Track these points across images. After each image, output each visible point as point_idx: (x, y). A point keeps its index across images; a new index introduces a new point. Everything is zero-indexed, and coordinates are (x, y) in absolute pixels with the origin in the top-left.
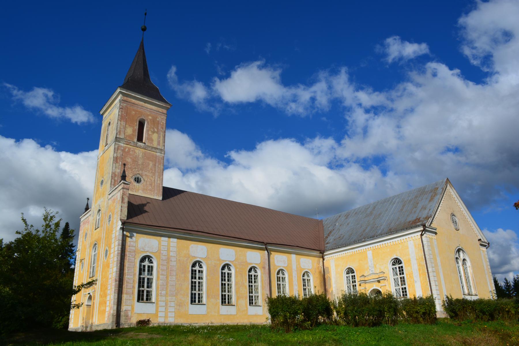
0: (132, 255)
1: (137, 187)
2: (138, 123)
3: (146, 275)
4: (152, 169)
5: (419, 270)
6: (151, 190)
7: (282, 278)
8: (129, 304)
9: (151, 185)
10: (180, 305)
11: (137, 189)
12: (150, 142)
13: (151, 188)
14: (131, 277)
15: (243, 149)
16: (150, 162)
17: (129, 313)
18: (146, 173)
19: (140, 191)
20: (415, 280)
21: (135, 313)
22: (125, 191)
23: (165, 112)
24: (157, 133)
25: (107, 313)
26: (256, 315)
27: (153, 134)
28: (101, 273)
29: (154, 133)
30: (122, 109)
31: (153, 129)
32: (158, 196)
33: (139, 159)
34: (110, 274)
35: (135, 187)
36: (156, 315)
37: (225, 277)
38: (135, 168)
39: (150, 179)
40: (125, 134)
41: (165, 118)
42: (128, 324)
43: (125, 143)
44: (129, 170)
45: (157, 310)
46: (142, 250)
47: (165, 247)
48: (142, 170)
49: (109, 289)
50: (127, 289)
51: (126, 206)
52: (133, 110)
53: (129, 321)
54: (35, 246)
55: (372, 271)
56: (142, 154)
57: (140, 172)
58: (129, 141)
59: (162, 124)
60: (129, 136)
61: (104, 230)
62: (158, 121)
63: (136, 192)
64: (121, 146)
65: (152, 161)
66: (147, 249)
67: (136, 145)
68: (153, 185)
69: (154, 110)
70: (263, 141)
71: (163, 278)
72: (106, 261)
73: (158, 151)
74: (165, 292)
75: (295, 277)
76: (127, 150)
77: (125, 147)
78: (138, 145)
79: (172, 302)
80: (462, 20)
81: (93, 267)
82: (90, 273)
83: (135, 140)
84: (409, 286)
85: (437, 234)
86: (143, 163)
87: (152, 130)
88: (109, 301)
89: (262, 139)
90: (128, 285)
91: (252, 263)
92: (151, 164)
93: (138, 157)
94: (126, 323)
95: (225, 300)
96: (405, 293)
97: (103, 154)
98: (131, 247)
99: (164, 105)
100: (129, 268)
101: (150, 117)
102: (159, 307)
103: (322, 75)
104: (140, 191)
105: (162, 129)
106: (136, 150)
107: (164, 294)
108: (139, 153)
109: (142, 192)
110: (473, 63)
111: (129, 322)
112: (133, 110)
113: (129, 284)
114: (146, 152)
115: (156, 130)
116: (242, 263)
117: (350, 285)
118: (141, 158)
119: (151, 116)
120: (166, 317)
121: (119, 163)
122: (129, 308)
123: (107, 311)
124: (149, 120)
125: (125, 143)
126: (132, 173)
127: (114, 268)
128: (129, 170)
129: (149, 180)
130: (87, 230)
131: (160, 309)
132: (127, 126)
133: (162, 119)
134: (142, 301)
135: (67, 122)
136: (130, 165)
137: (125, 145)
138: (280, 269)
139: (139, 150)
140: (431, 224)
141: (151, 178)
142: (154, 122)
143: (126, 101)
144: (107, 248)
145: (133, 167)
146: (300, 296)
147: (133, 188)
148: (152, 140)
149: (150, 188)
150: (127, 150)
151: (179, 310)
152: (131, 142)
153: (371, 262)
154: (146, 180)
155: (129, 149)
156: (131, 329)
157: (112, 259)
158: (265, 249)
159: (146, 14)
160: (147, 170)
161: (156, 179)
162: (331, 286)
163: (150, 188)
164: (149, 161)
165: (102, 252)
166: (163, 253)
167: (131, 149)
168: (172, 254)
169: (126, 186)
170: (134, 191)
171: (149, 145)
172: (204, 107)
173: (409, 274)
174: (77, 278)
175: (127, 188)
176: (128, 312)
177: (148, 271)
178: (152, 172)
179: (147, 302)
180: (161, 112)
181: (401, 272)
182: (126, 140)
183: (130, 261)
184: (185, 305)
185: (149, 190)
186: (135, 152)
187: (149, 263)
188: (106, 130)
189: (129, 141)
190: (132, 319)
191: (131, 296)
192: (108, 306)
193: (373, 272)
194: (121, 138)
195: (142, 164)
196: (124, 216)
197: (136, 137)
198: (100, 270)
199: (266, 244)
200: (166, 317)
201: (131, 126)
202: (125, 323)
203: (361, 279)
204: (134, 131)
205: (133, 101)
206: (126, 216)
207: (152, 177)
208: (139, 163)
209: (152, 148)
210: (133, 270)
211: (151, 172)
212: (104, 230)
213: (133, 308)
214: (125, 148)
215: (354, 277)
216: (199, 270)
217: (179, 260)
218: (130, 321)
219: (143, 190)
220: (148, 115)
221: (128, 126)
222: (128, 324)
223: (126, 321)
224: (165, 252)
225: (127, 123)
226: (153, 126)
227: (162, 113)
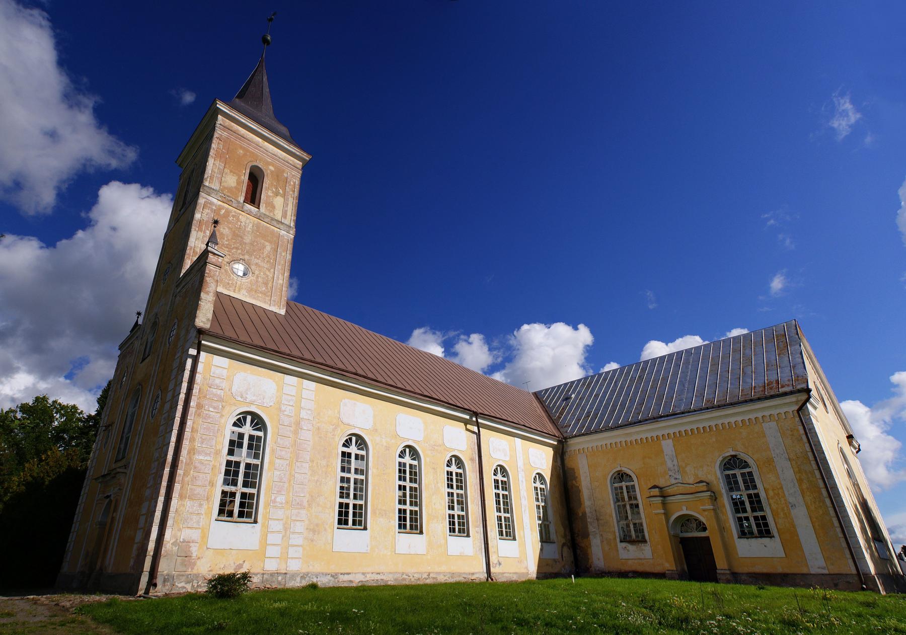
0: (214, 408)
1: (239, 283)
2: (248, 171)
3: (742, 495)
4: (269, 257)
5: (800, 481)
6: (264, 294)
7: (500, 512)
8: (195, 525)
9: (266, 284)
10: (315, 529)
11: (237, 286)
12: (268, 208)
13: (265, 290)
14: (208, 458)
15: (170, 196)
16: (267, 244)
17: (194, 550)
18: (256, 261)
19: (244, 292)
20: (790, 503)
21: (602, 535)
22: (212, 270)
23: (298, 166)
24: (284, 196)
25: (135, 546)
26: (462, 557)
27: (276, 198)
28: (138, 449)
29: (277, 196)
30: (220, 140)
31: (276, 188)
32: (277, 307)
33: (246, 234)
34: (157, 449)
35: (234, 282)
36: (261, 554)
37: (456, 481)
38: (237, 248)
39: (265, 274)
40: (222, 185)
41: (299, 176)
42: (188, 577)
43: (220, 199)
44: (223, 248)
45: (264, 543)
46: (239, 399)
47: (290, 398)
48: (251, 255)
49: (149, 486)
50: (194, 487)
51: (210, 300)
52: (241, 147)
53: (190, 570)
54: (813, 505)
55: (676, 479)
56: (253, 226)
57: (246, 257)
58: (229, 198)
59: (292, 183)
60: (230, 189)
61: (158, 358)
62: (287, 178)
63: (235, 292)
64: (212, 203)
65: (270, 242)
66: (250, 398)
67: (243, 208)
68: (270, 285)
69: (279, 158)
70: (298, 288)
71: (282, 466)
72: (153, 421)
73: (282, 227)
74: (283, 497)
75: (522, 481)
76: (223, 212)
77: (219, 205)
78: (245, 208)
79: (298, 523)
80: (295, 277)
81: (126, 438)
82: (119, 452)
83: (242, 199)
84: (775, 514)
85: (340, 498)
86: (254, 242)
87: (274, 190)
88: (144, 517)
89: (732, 329)
90: (199, 477)
91: (409, 440)
92: (268, 247)
93: (245, 229)
94: (183, 575)
95: (458, 527)
96: (343, 518)
97: (175, 224)
98: (214, 390)
99: (298, 153)
100: (204, 437)
101: (272, 168)
102: (279, 542)
103: (151, 189)
104: (244, 292)
105: (291, 193)
106: (240, 217)
107: (282, 503)
108: (246, 223)
109: (247, 294)
110: (207, 293)
111: (189, 571)
112: (241, 147)
113: (201, 475)
114: (260, 223)
115: (281, 191)
116: (436, 447)
117: (623, 503)
118: (250, 233)
119: (273, 166)
120: (285, 557)
121: (205, 232)
122: (194, 535)
123: (137, 543)
124: (269, 171)
125: (220, 199)
126: (229, 255)
127: (476, 428)
128: (225, 249)
129: (262, 274)
130: (127, 367)
131: (271, 538)
132: (226, 170)
133: (294, 175)
134: (229, 519)
135: (667, 340)
136: (226, 241)
137: (220, 203)
138: (696, 520)
139: (247, 218)
140: (726, 570)
141: (268, 273)
142: (278, 176)
143: (229, 129)
144: (160, 393)
145: (233, 246)
146: (627, 551)
147: (229, 284)
148: (274, 207)
149: (264, 289)
150: (223, 212)
151: (312, 541)
152: (233, 200)
153: (673, 461)
154: (257, 272)
155: (228, 212)
156: (99, 413)
157: (166, 415)
158: (476, 424)
159: (765, 546)
160: (260, 256)
161: (275, 276)
162: (581, 504)
163: (264, 289)
164: (265, 241)
165: (147, 402)
166: (285, 411)
167: (231, 212)
168: (303, 414)
169: (214, 260)
170: (231, 289)
171: (267, 213)
172: (17, 363)
173: (773, 490)
174: (87, 491)
175: (218, 264)
176: (191, 544)
177: (250, 447)
178: (270, 262)
179: (354, 527)
180: (293, 164)
181: (344, 510)
182: (223, 195)
183: (209, 421)
184: (325, 530)
185: (261, 292)
186: (238, 219)
187: (253, 430)
188: (792, 361)
189: (229, 198)
190: (199, 563)
191: (202, 505)
192: (141, 528)
193: (677, 481)
194: (213, 189)
195: (252, 244)
196: (204, 320)
197: (244, 194)
198: (118, 522)
199: (476, 414)
200: (285, 557)
201: (234, 173)
202: (178, 575)
203: (652, 494)
204: (239, 182)
205: (243, 131)
206: (208, 320)
207: (269, 271)
208: (245, 241)
209: (272, 219)
210: (214, 441)
211: (267, 262)
212: (158, 358)
213: (205, 536)
214: (220, 208)
215: (631, 489)
216: (355, 479)
217: (319, 429)
218: (192, 569)
219: (250, 291)
220: (268, 164)
221: (229, 171)
222: (188, 577)
223: (184, 569)
224: (291, 408)
225: (227, 166)
226: (275, 184)
227: (294, 167)
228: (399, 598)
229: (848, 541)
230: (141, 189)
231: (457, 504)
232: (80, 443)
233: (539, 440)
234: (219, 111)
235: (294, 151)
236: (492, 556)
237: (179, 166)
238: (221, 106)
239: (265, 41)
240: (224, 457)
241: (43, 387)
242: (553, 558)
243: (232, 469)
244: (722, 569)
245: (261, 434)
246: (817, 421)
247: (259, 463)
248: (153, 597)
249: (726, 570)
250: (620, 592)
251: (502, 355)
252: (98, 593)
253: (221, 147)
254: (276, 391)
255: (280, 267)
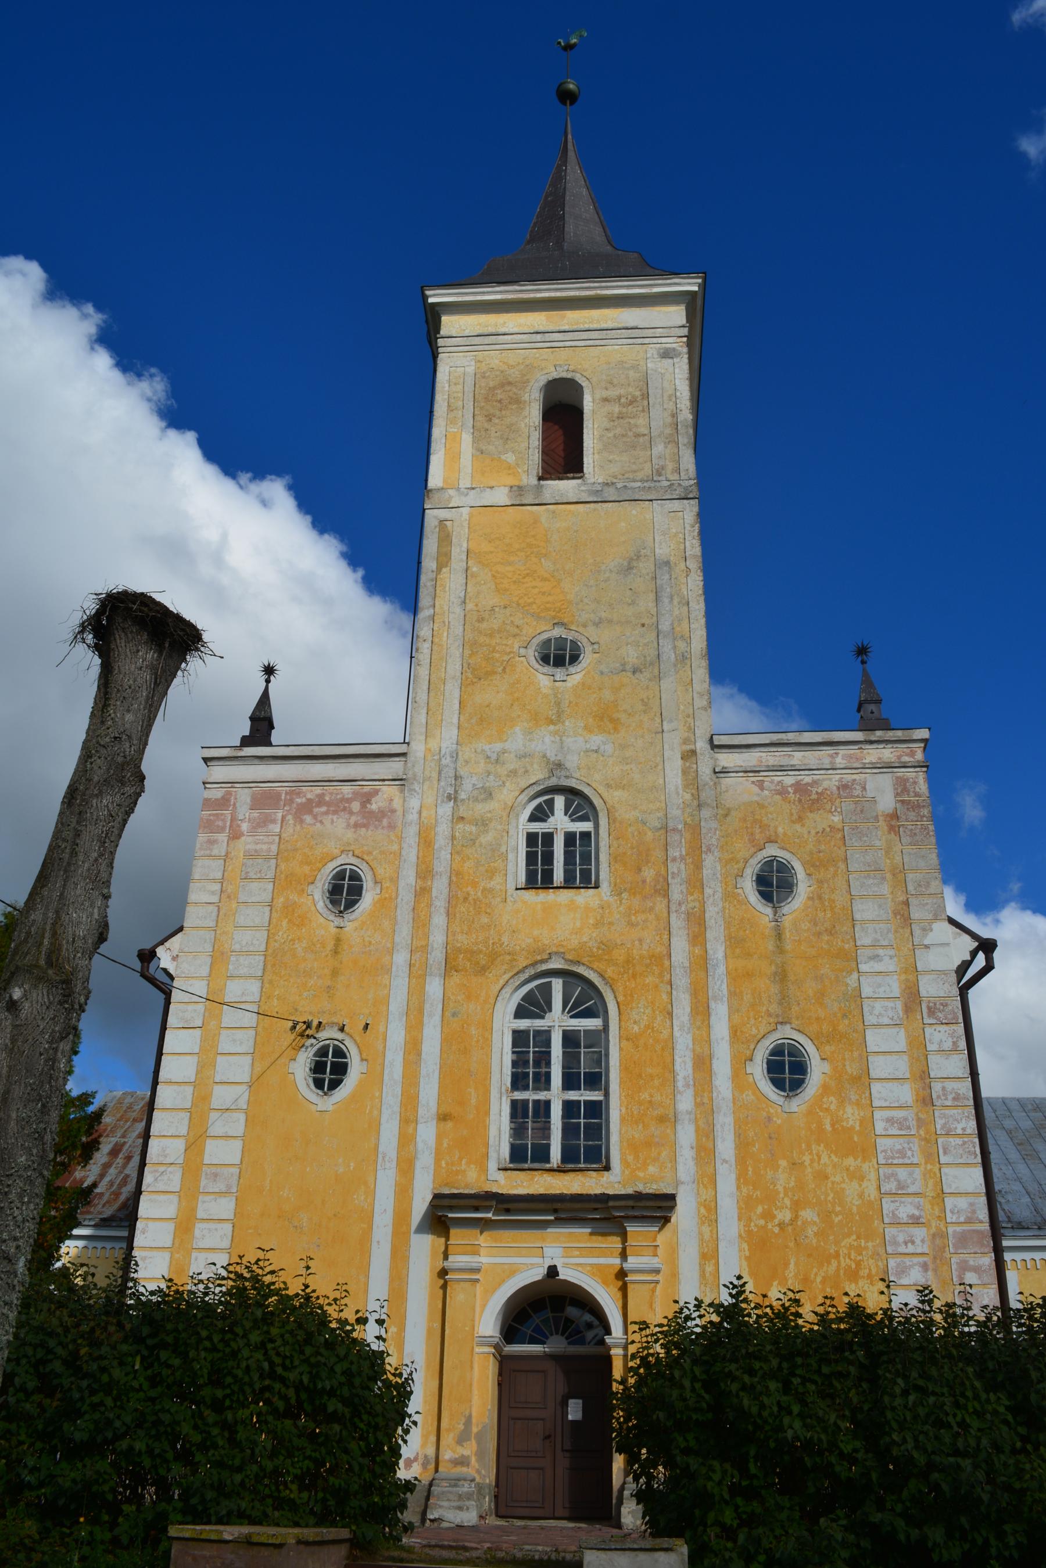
61: (698, 937)
104: (826, 1067)
110: (695, 556)
228: (78, 1522)
229: (406, 1063)
230: (163, 430)
231: (476, 1253)
232: (58, 1335)
233: (566, 863)
234: (437, 308)
235: (498, 297)
236: (467, 1186)
237: (206, 760)
238: (436, 297)
239: (566, 97)
240: (523, 825)
241: (749, 878)
242: (435, 1122)
243: (582, 1121)
244: (450, 1547)
245: (586, 826)
246: (259, 1248)
247: (592, 830)
248: (438, 938)
249: (814, 1324)
250: (756, 801)
251: (677, 864)
252: (360, 573)
253: (815, 1270)
254: (899, 1005)
255: (433, 765)
